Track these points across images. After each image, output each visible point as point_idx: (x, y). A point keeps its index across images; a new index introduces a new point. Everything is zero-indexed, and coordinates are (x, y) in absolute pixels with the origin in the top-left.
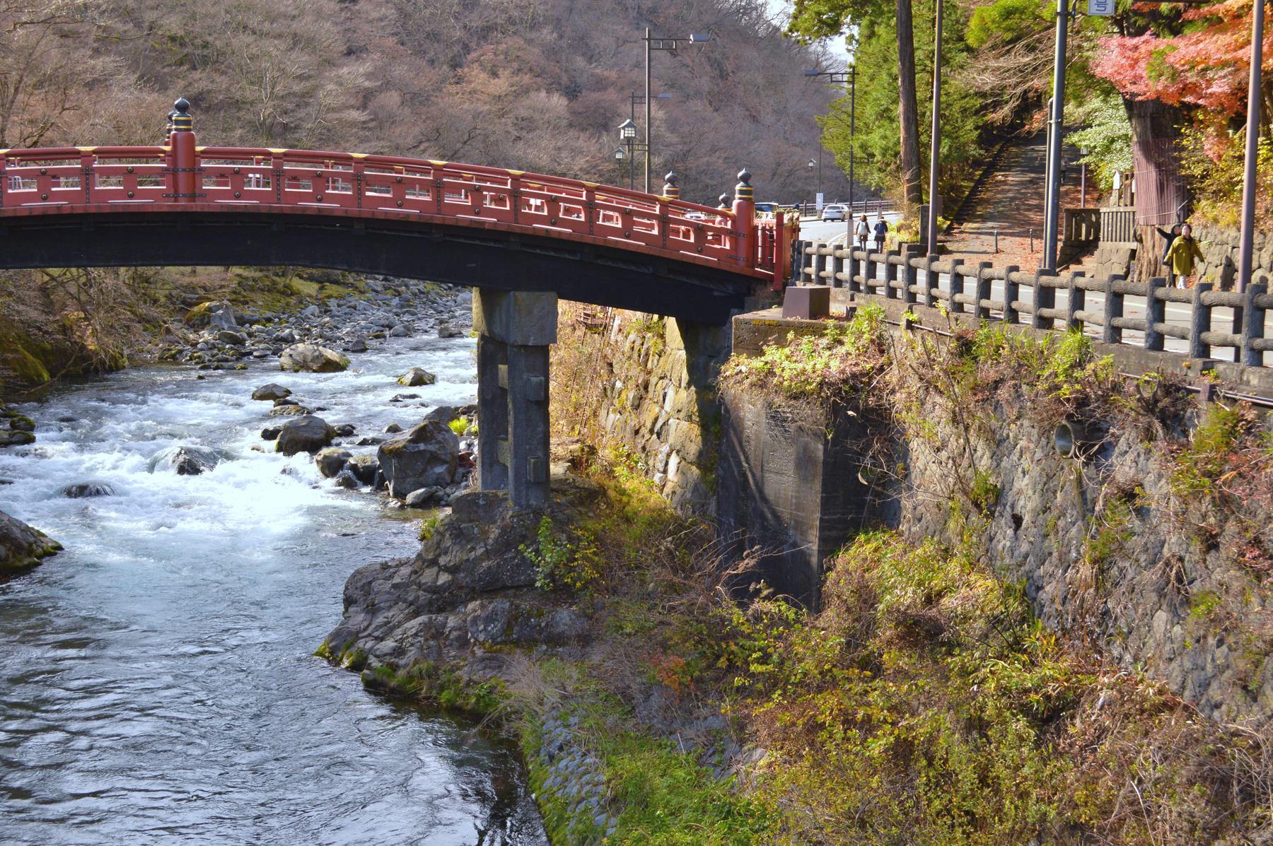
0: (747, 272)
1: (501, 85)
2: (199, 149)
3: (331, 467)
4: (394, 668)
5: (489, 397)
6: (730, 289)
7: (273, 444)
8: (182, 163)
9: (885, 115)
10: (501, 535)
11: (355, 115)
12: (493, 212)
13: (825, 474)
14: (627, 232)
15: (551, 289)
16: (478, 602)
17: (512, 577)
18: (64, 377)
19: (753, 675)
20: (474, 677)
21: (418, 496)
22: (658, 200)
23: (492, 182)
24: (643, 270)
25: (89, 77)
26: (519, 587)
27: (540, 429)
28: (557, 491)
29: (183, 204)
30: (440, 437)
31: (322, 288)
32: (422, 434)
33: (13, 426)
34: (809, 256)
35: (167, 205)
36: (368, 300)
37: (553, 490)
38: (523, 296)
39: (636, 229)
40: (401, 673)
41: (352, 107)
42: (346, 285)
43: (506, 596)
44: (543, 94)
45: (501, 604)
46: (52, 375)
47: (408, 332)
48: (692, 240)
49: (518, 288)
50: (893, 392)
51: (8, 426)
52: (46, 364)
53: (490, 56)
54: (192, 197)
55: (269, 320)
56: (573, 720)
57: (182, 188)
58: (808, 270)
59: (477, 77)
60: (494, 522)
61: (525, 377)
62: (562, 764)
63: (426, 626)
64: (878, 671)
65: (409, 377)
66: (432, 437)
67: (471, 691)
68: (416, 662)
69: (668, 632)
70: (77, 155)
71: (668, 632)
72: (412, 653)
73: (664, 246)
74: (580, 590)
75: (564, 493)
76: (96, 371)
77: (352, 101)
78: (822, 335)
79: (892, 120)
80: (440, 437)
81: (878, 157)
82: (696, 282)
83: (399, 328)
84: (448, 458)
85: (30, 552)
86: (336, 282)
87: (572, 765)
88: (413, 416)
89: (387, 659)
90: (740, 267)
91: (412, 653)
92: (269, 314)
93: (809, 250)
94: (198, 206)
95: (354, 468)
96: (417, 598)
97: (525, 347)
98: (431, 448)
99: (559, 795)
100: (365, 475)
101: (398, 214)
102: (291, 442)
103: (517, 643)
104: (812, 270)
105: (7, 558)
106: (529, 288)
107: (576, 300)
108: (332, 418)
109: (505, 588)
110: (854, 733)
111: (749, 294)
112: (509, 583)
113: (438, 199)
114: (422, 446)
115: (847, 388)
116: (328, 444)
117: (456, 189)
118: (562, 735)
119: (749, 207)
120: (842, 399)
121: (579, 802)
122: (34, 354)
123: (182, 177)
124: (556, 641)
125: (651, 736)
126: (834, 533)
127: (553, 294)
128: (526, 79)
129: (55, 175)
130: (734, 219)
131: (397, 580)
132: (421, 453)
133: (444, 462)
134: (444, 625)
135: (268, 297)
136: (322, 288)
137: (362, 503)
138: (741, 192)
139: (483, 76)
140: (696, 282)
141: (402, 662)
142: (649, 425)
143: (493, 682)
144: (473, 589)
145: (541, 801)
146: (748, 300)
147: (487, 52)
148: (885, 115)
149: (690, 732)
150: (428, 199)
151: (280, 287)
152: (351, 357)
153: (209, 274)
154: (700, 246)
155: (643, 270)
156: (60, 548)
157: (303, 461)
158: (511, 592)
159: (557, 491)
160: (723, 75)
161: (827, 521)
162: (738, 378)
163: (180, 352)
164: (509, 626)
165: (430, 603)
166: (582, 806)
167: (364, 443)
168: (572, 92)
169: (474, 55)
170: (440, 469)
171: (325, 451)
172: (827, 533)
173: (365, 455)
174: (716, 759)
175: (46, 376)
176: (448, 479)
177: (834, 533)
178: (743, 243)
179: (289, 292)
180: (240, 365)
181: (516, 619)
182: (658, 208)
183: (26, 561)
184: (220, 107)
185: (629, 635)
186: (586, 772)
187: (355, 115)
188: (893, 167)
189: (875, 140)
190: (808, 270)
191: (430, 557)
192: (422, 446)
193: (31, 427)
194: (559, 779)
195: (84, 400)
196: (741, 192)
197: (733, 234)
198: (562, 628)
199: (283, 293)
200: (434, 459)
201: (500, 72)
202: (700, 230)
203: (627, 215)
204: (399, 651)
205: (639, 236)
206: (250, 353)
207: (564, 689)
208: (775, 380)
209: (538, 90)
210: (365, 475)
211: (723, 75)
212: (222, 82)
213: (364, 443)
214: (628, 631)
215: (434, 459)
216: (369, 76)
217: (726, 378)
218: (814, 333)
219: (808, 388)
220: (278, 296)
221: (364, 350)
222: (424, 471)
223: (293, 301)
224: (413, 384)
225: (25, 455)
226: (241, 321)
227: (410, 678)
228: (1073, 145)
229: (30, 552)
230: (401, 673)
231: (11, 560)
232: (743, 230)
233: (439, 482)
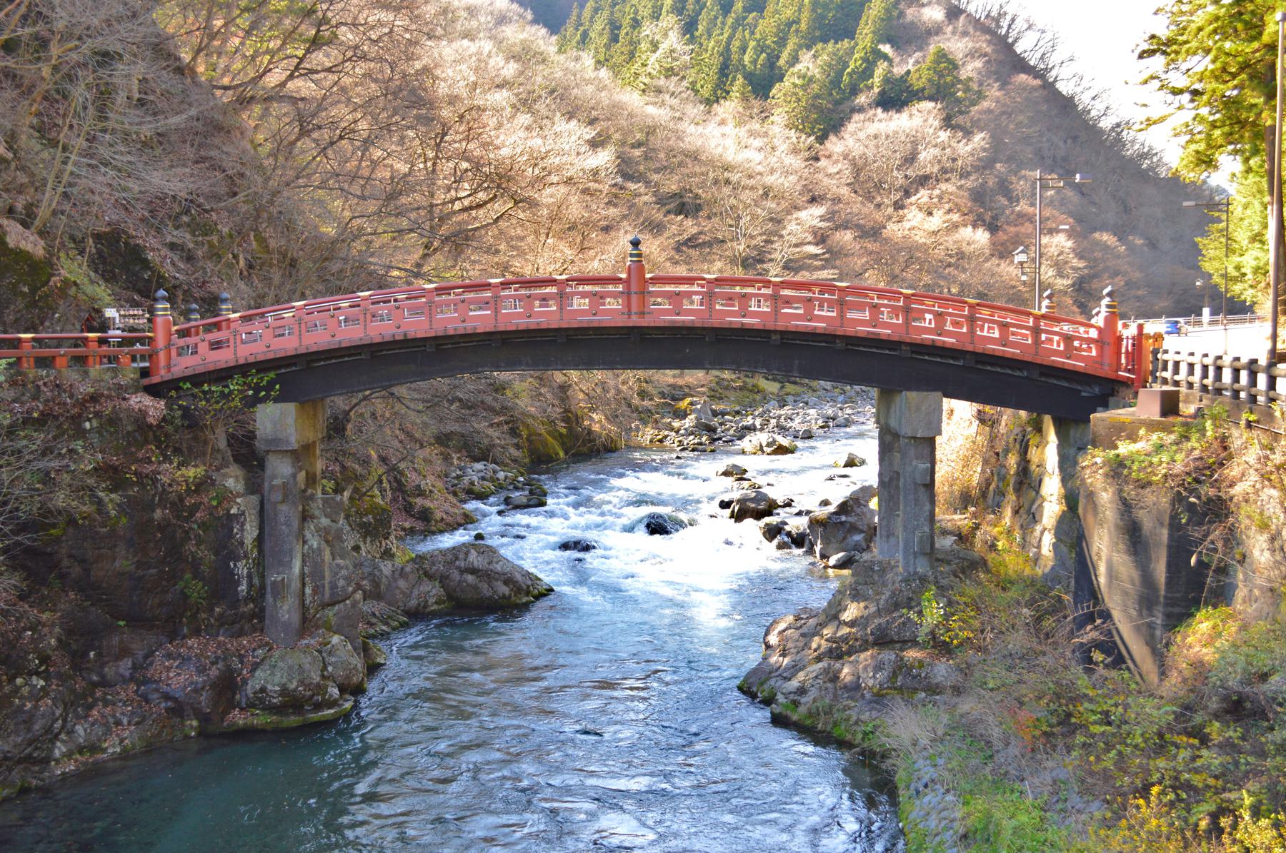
0: (1111, 375)
1: (937, 221)
2: (648, 276)
3: (772, 533)
4: (796, 704)
5: (886, 480)
6: (1097, 390)
7: (728, 512)
8: (634, 288)
9: (1258, 238)
10: (891, 597)
11: (812, 249)
12: (889, 324)
13: (1169, 556)
14: (1003, 341)
15: (935, 389)
16: (869, 653)
17: (898, 633)
18: (573, 455)
19: (1093, 736)
20: (862, 717)
21: (838, 560)
22: (1031, 314)
23: (889, 300)
24: (1018, 373)
25: (603, 223)
26: (904, 642)
27: (927, 507)
28: (942, 561)
29: (635, 321)
30: (859, 511)
31: (783, 387)
32: (844, 508)
33: (531, 492)
34: (1166, 362)
35: (621, 321)
36: (819, 397)
37: (938, 560)
38: (913, 396)
39: (1012, 338)
40: (802, 709)
41: (809, 243)
42: (802, 385)
43: (893, 649)
44: (970, 228)
45: (888, 656)
46: (566, 453)
47: (847, 423)
48: (1062, 348)
49: (909, 389)
50: (1232, 485)
51: (527, 493)
52: (563, 445)
53: (925, 199)
54: (642, 314)
55: (738, 413)
56: (941, 762)
57: (634, 309)
58: (1165, 374)
59: (913, 217)
60: (886, 586)
61: (914, 463)
62: (926, 799)
63: (826, 671)
64: (1204, 740)
65: (842, 462)
66: (852, 510)
67: (858, 729)
68: (815, 700)
69: (1023, 690)
70: (487, 286)
71: (1023, 690)
72: (813, 693)
73: (1037, 354)
74: (957, 647)
75: (949, 563)
76: (598, 451)
77: (810, 238)
78: (1171, 432)
79: (1263, 242)
80: (859, 511)
81: (1250, 276)
82: (1066, 384)
83: (840, 420)
84: (865, 528)
85: (528, 593)
86: (795, 383)
87: (935, 800)
88: (839, 493)
89: (792, 696)
90: (1106, 371)
91: (813, 693)
92: (737, 408)
93: (1165, 357)
94: (646, 322)
95: (789, 534)
96: (819, 646)
97: (915, 438)
98: (851, 519)
99: (920, 826)
100: (798, 540)
101: (807, 327)
102: (741, 512)
103: (900, 690)
104: (1168, 375)
105: (510, 596)
106: (918, 389)
107: (972, 401)
108: (777, 494)
109: (892, 642)
110: (1080, 826)
111: (1112, 395)
112: (896, 638)
113: (842, 315)
114: (843, 518)
115: (1190, 480)
116: (770, 514)
117: (860, 307)
118: (928, 773)
119: (1111, 320)
120: (1186, 489)
121: (937, 835)
122: (554, 438)
123: (634, 298)
124: (934, 690)
125: (1001, 781)
126: (1177, 610)
127: (940, 394)
128: (956, 217)
129: (602, 296)
130: (1099, 329)
131: (804, 630)
132: (842, 523)
133: (862, 531)
134: (840, 671)
135: (739, 394)
136: (783, 387)
137: (797, 561)
138: (1108, 306)
139: (921, 215)
140: (1066, 384)
141: (803, 700)
142: (1026, 506)
143: (878, 722)
144: (866, 641)
145: (906, 830)
146: (1112, 400)
147: (923, 195)
148: (1258, 238)
149: (1036, 781)
150: (834, 314)
151: (749, 386)
152: (799, 444)
153: (695, 377)
154: (1069, 352)
155: (1018, 373)
156: (552, 590)
157: (752, 527)
158: (898, 646)
159: (942, 561)
160: (1127, 210)
161: (1171, 599)
162: (1094, 468)
163: (666, 437)
164: (894, 675)
165: (830, 651)
166: (938, 839)
167: (799, 514)
168: (993, 228)
169: (913, 199)
170: (858, 538)
171: (767, 520)
172: (1170, 609)
173: (797, 524)
174: (1060, 806)
175: (562, 454)
176: (864, 545)
177: (1177, 610)
178: (1108, 351)
179: (756, 390)
180: (709, 448)
181: (900, 669)
182: (1031, 320)
183: (524, 600)
184: (709, 244)
185: (992, 690)
186: (945, 809)
187: (812, 249)
188: (1263, 285)
189: (1248, 262)
190: (1165, 374)
191: (833, 612)
192: (843, 518)
193: (545, 494)
194: (922, 813)
195: (585, 472)
196: (1108, 306)
197: (1099, 342)
198: (939, 679)
199: (751, 391)
200: (853, 529)
201: (935, 212)
202: (1068, 339)
203: (1004, 326)
204: (802, 691)
205: (1014, 345)
206: (720, 439)
207: (935, 733)
208: (1126, 472)
209: (965, 226)
210: (798, 540)
211: (1127, 210)
212: (707, 225)
213: (799, 514)
214: (991, 686)
215: (853, 529)
216: (822, 218)
217: (1083, 468)
218: (1163, 430)
219: (1154, 478)
220: (747, 393)
221: (810, 437)
222: (844, 538)
223: (758, 397)
224: (845, 466)
225: (538, 514)
226: (715, 414)
227: (810, 714)
228: (138, 245)
229: (528, 593)
230: (802, 709)
231: (513, 598)
232: (1109, 339)
233: (857, 547)
